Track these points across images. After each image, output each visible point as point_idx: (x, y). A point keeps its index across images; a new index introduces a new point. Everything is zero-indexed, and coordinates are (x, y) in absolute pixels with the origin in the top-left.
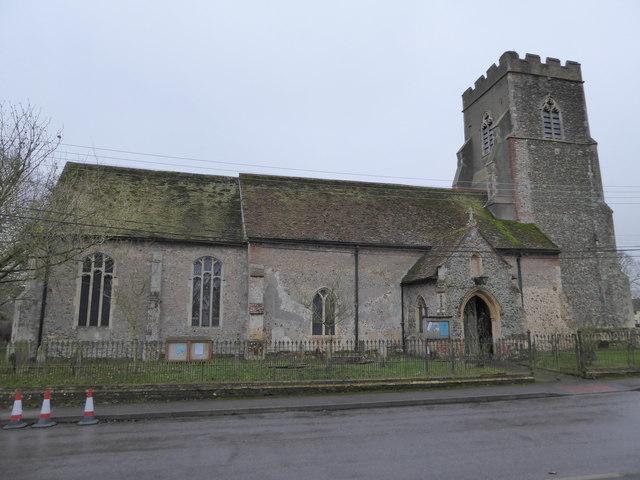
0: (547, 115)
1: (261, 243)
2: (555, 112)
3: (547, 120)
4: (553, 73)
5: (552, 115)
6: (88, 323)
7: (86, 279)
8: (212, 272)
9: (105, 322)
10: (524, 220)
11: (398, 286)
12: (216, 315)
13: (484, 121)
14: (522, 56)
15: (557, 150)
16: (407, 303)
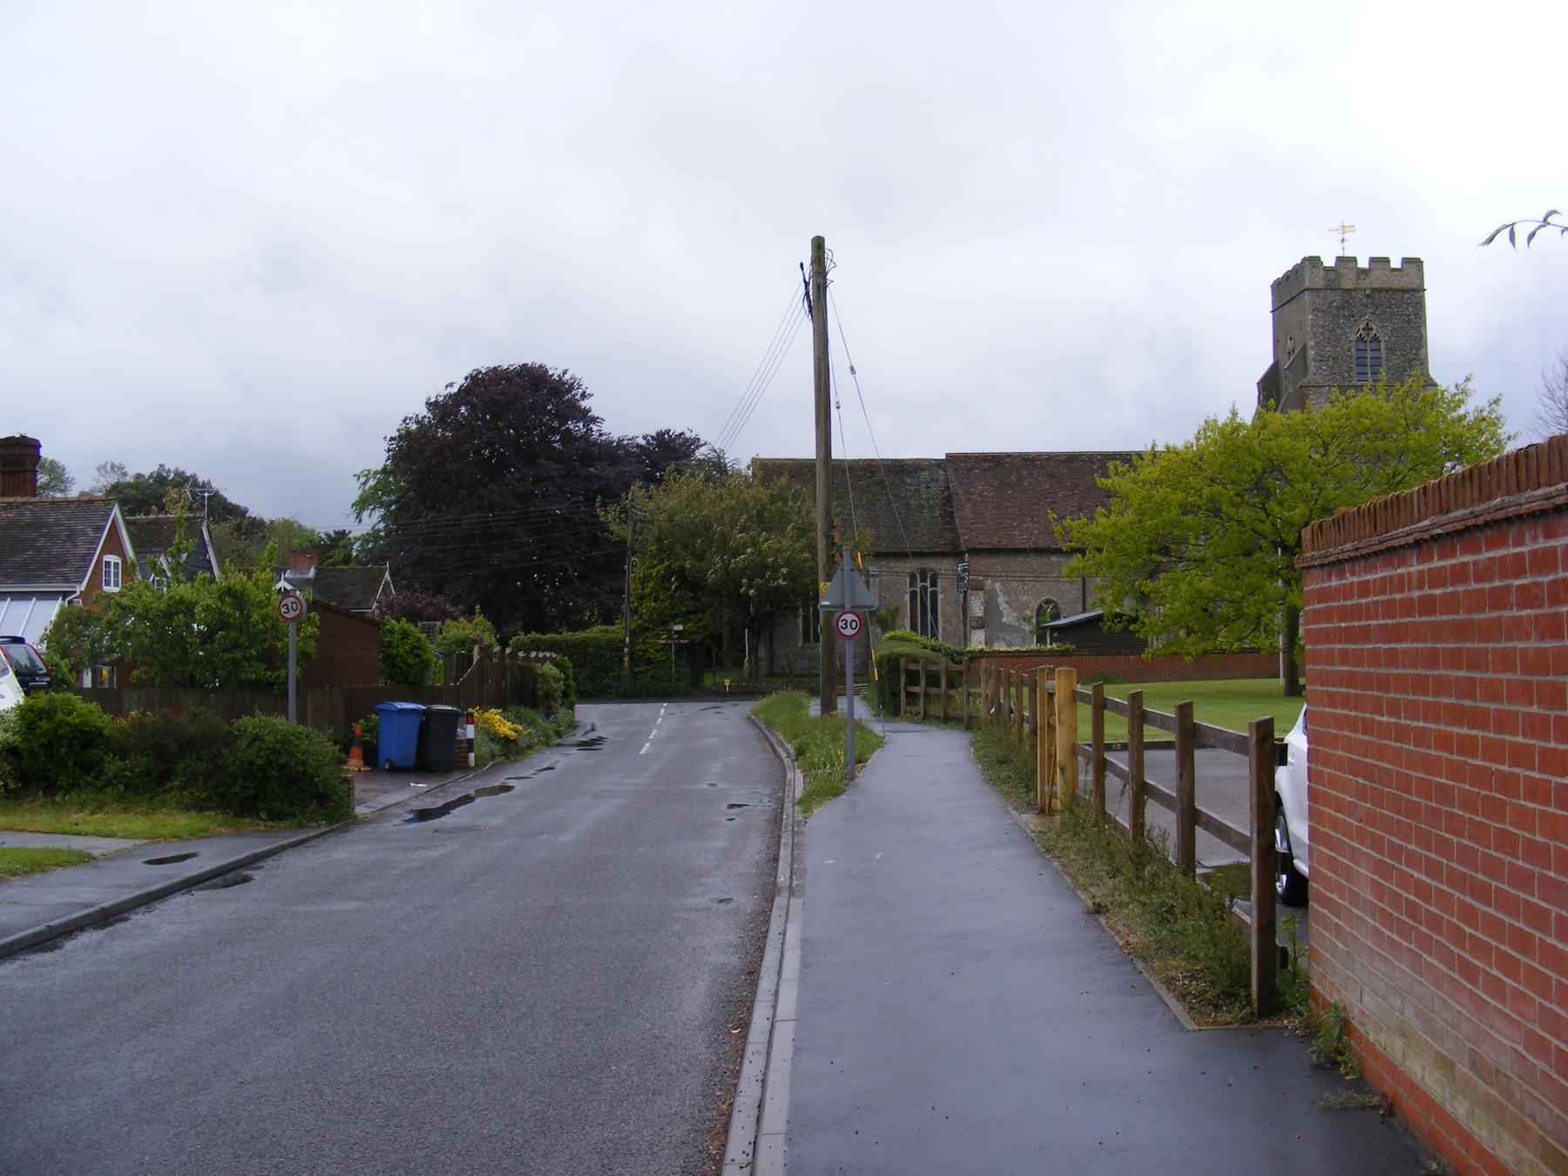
2: (1376, 339)
4: (1378, 280)
7: (913, 595)
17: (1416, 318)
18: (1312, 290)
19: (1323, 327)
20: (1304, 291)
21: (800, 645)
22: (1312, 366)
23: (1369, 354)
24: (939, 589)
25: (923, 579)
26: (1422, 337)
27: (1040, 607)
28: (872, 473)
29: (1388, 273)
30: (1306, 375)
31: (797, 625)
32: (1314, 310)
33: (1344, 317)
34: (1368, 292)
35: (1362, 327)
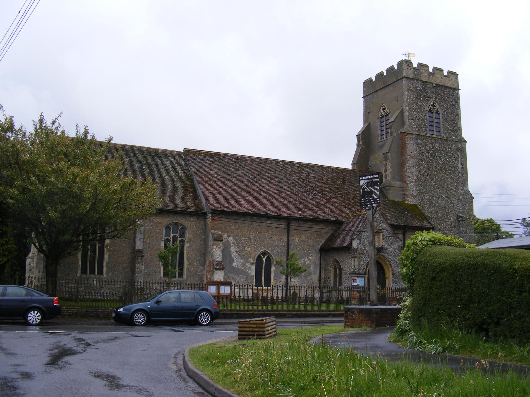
0: (431, 115)
1: (219, 214)
2: (437, 112)
3: (431, 119)
4: (437, 80)
5: (435, 115)
6: (88, 272)
8: (178, 235)
9: (100, 272)
10: (410, 201)
11: (317, 251)
12: (182, 269)
13: (382, 111)
14: (415, 65)
15: (437, 144)
16: (323, 265)
17: (456, 104)
18: (408, 78)
19: (413, 100)
20: (402, 78)
21: (78, 275)
22: (407, 121)
23: (435, 120)
24: (186, 239)
25: (175, 232)
26: (459, 115)
27: (259, 257)
28: (135, 154)
29: (443, 77)
30: (403, 127)
31: (78, 260)
32: (408, 90)
33: (423, 97)
34: (434, 85)
35: (431, 104)
